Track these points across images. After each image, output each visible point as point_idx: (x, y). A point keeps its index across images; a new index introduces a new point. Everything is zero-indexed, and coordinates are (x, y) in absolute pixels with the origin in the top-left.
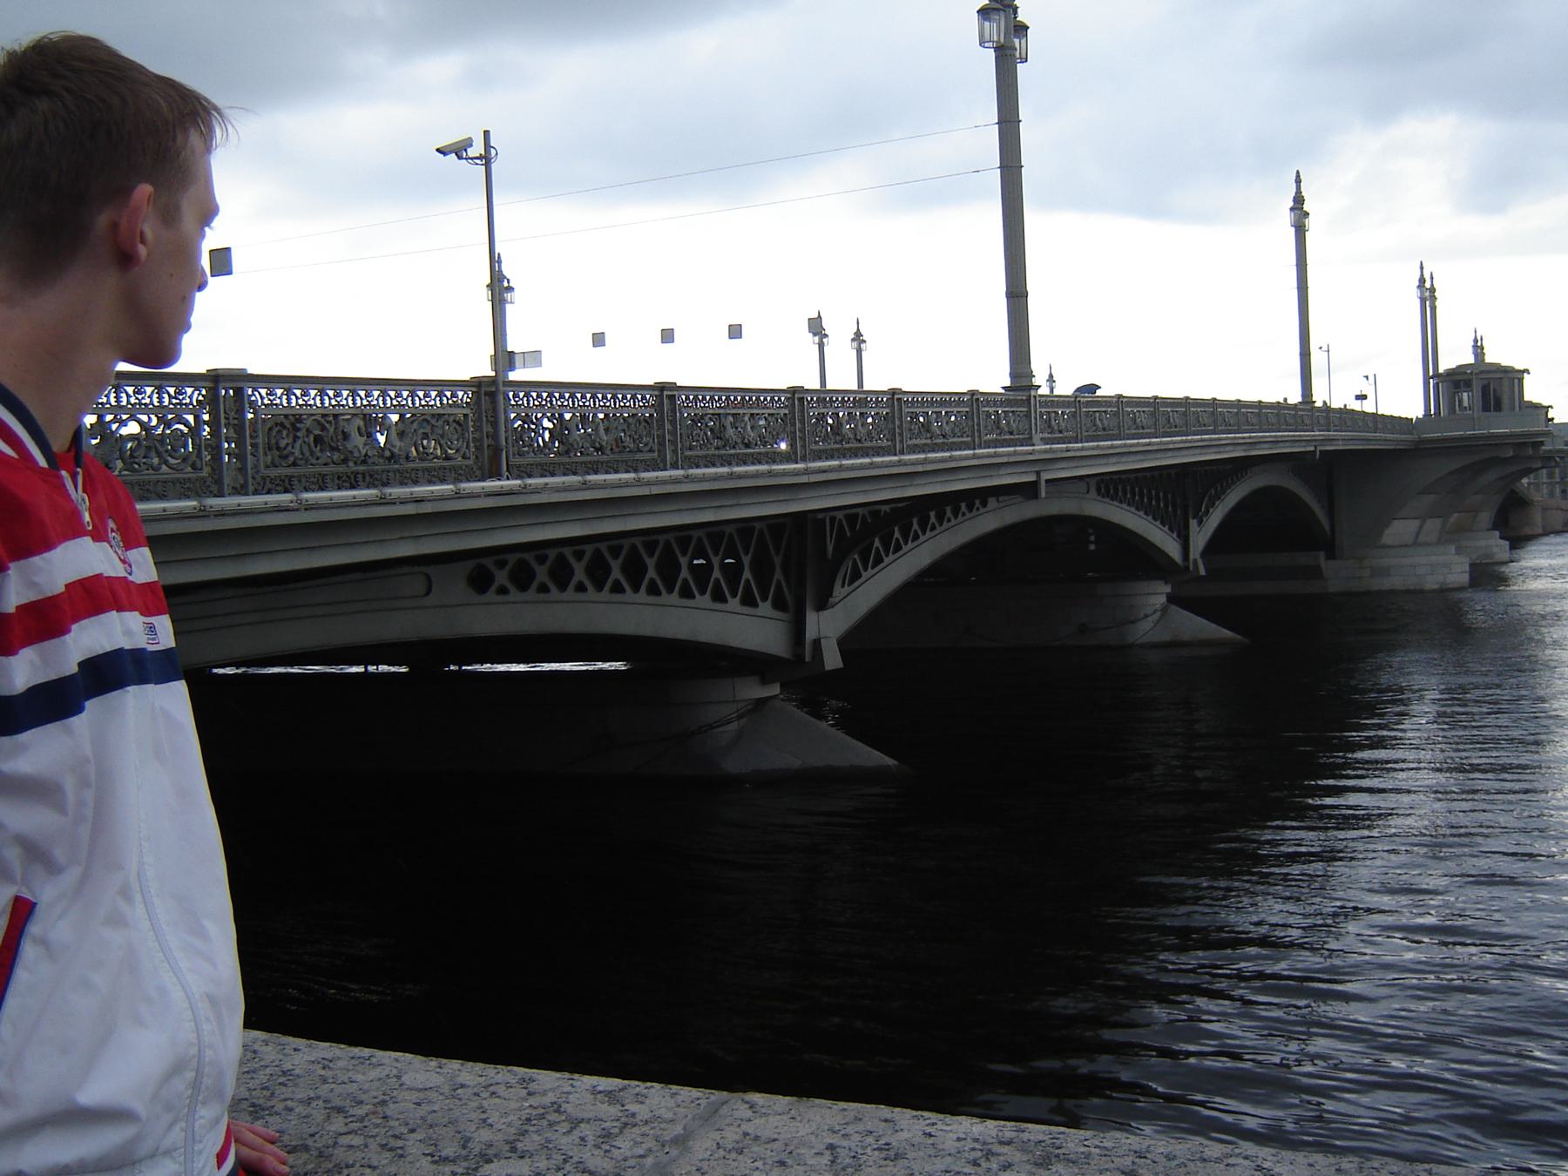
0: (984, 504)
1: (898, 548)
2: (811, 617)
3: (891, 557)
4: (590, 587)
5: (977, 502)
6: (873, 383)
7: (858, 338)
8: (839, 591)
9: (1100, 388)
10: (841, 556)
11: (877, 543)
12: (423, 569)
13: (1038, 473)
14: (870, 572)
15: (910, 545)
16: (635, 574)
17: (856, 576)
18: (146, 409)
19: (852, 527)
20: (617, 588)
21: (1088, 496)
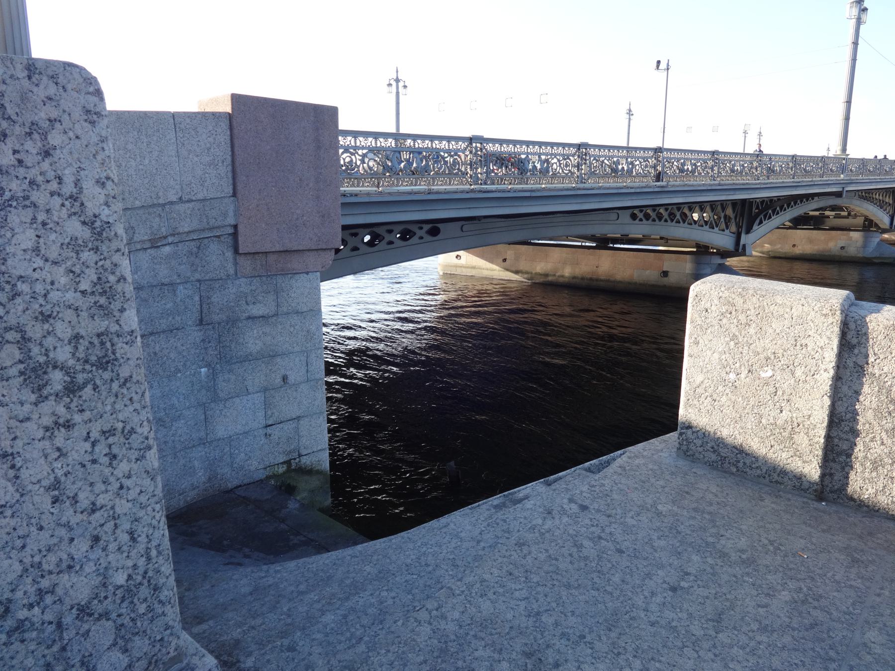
0: (813, 199)
1: (778, 213)
2: (743, 236)
3: (775, 216)
4: (657, 220)
5: (805, 200)
6: (856, 151)
7: (760, 134)
8: (755, 227)
9: (885, 156)
10: (757, 215)
11: (770, 211)
12: (617, 211)
13: (843, 188)
14: (766, 221)
15: (783, 212)
16: (672, 216)
17: (761, 222)
18: (559, 155)
19: (762, 206)
20: (678, 222)
21: (618, 222)
